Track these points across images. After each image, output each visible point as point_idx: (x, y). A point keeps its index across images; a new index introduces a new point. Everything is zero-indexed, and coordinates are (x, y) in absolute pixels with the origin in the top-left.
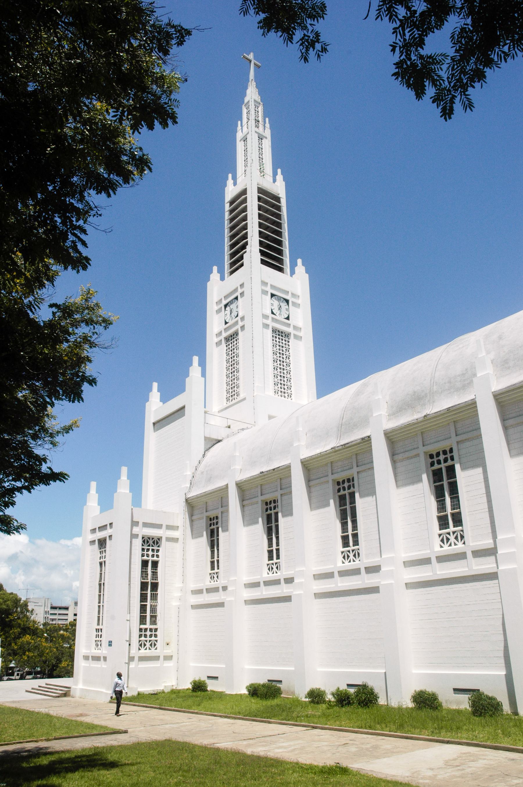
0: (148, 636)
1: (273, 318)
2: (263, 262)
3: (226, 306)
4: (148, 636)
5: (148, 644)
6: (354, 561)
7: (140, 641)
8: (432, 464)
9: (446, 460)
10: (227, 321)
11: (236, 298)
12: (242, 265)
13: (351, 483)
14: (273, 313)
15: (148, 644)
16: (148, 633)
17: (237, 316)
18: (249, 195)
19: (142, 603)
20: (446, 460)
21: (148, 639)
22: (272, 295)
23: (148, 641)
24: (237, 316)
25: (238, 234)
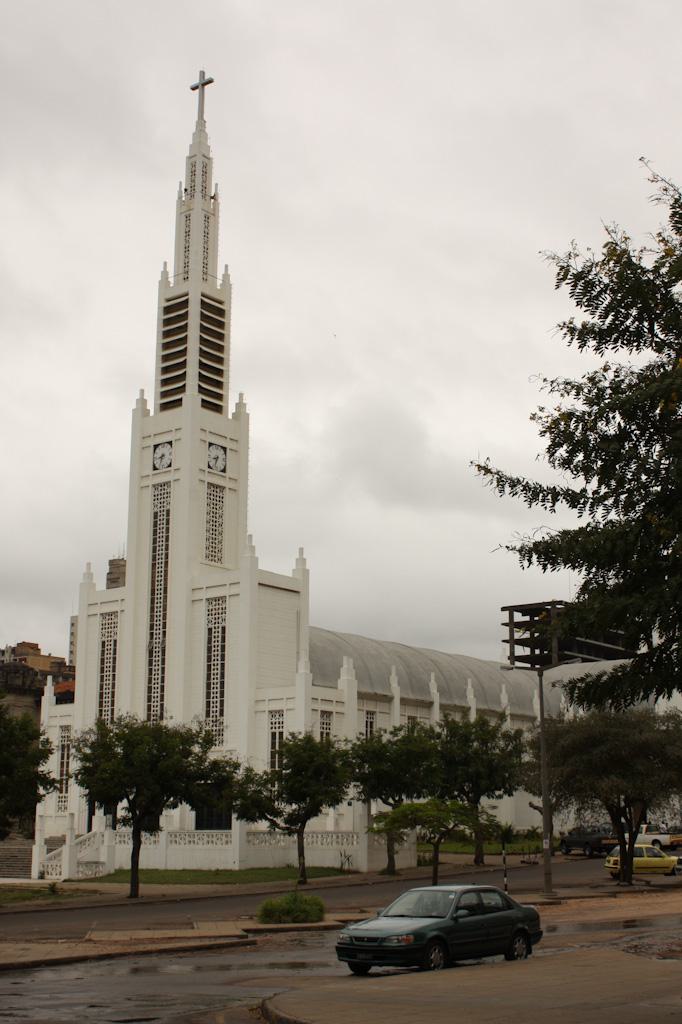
3: (156, 447)
10: (157, 466)
11: (170, 443)
14: (209, 467)
22: (211, 444)
24: (170, 466)
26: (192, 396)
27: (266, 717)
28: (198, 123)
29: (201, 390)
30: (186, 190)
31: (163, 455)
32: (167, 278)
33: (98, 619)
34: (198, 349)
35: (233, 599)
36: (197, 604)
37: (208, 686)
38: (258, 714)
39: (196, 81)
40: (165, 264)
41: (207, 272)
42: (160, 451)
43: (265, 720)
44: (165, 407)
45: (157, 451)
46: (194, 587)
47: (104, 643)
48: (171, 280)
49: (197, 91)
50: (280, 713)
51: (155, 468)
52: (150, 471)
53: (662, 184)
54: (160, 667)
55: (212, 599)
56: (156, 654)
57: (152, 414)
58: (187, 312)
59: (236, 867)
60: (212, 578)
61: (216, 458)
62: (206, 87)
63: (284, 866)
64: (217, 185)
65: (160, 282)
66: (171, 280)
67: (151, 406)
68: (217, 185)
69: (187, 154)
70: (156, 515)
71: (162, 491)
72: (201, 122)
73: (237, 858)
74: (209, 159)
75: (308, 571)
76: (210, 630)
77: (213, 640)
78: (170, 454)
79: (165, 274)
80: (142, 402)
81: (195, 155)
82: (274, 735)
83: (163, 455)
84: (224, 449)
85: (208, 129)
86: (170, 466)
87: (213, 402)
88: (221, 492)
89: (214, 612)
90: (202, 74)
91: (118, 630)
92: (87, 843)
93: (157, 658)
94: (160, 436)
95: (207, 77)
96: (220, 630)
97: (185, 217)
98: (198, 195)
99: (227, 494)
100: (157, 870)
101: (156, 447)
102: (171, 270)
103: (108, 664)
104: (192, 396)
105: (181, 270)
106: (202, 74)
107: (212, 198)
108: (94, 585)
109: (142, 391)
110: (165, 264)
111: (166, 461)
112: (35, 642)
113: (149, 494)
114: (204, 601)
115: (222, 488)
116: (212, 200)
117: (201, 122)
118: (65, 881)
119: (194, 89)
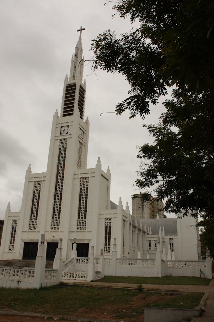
3: (62, 127)
5: (107, 252)
8: (106, 224)
9: (109, 224)
10: (62, 133)
11: (68, 126)
15: (107, 252)
20: (109, 224)
22: (81, 129)
24: (67, 133)
27: (104, 220)
28: (79, 39)
31: (65, 130)
32: (67, 78)
35: (91, 178)
36: (76, 180)
39: (79, 28)
40: (67, 74)
42: (63, 129)
44: (64, 115)
45: (62, 128)
48: (69, 79)
49: (80, 32)
50: (110, 219)
52: (59, 135)
55: (82, 178)
56: (58, 196)
57: (59, 117)
59: (160, 276)
61: (81, 134)
62: (82, 31)
63: (59, 283)
64: (84, 57)
65: (65, 79)
66: (69, 79)
67: (59, 115)
68: (84, 57)
69: (76, 46)
70: (60, 149)
71: (63, 142)
72: (80, 40)
73: (159, 271)
75: (10, 210)
76: (81, 189)
78: (68, 129)
79: (67, 77)
82: (106, 227)
83: (65, 130)
84: (83, 132)
85: (82, 42)
86: (67, 133)
90: (81, 27)
92: (71, 262)
94: (66, 124)
95: (83, 28)
99: (83, 146)
100: (112, 276)
101: (62, 127)
102: (69, 77)
105: (72, 76)
106: (81, 27)
108: (31, 172)
109: (57, 110)
110: (67, 74)
111: (66, 132)
113: (58, 142)
114: (79, 178)
115: (82, 144)
117: (80, 40)
118: (92, 281)
119: (78, 31)
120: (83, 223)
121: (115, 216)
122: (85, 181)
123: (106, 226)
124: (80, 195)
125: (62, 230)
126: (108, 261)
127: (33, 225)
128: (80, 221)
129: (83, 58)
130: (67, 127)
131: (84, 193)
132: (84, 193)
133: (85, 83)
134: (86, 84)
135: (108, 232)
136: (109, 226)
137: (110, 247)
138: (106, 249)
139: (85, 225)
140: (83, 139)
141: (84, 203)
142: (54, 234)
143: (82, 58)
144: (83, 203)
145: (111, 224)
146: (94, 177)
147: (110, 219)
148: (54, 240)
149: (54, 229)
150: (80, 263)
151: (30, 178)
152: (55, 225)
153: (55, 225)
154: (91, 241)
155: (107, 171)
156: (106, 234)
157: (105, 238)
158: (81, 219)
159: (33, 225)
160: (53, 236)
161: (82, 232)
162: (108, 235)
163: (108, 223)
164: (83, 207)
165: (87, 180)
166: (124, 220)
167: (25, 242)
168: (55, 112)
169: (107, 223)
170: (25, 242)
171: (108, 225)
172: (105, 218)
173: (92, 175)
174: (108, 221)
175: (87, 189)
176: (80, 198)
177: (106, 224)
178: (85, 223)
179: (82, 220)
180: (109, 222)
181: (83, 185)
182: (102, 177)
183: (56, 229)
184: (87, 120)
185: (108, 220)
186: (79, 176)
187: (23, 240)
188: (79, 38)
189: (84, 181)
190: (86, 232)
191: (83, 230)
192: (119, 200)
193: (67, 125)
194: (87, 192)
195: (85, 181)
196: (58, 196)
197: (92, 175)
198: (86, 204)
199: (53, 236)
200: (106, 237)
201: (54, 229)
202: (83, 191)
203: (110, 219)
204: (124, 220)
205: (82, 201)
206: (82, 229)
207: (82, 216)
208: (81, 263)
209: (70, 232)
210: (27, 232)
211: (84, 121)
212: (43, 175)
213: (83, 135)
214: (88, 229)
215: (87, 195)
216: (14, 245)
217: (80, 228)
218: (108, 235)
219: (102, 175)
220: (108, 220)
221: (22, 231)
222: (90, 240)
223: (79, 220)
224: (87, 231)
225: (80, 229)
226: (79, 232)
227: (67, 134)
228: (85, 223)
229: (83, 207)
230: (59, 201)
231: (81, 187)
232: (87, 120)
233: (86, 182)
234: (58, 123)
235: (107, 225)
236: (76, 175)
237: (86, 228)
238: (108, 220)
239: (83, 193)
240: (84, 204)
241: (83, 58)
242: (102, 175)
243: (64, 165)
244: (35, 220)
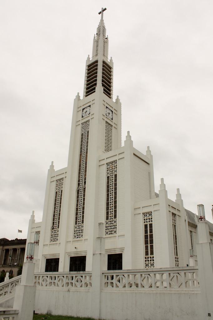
0: (149, 261)
1: (106, 117)
2: (104, 93)
3: (83, 109)
4: (149, 261)
5: (150, 265)
6: (151, 267)
7: (146, 263)
8: (145, 222)
9: (149, 221)
10: (84, 116)
11: (90, 106)
12: (95, 92)
13: (82, 231)
14: (106, 115)
15: (150, 265)
16: (149, 259)
17: (90, 114)
18: (99, 63)
19: (52, 270)
20: (149, 221)
21: (149, 262)
22: (107, 107)
23: (149, 263)
24: (90, 114)
25: (93, 79)
26: (99, 88)
27: (141, 217)
29: (103, 85)
30: (97, 34)
31: (86, 111)
33: (55, 182)
34: (102, 76)
36: (101, 167)
37: (108, 204)
38: (136, 216)
41: (105, 53)
42: (85, 111)
43: (141, 218)
46: (100, 160)
47: (56, 192)
49: (101, 14)
50: (150, 213)
51: (83, 117)
52: (81, 118)
53: (10, 285)
54: (58, 221)
55: (109, 163)
56: (81, 192)
58: (97, 79)
60: (108, 157)
62: (104, 12)
64: (107, 36)
65: (87, 61)
68: (107, 36)
69: (97, 27)
70: (82, 135)
71: (86, 124)
74: (105, 28)
76: (108, 177)
77: (56, 211)
78: (90, 110)
80: (78, 96)
81: (100, 26)
82: (146, 226)
83: (86, 111)
87: (108, 91)
88: (111, 126)
89: (77, 232)
91: (63, 186)
93: (81, 194)
95: (104, 8)
96: (114, 176)
97: (96, 42)
98: (101, 35)
99: (113, 129)
101: (83, 109)
103: (58, 201)
104: (99, 88)
107: (106, 39)
111: (88, 113)
112: (160, 179)
113: (79, 128)
115: (112, 126)
116: (106, 39)
119: (100, 13)
120: (113, 225)
121: (156, 208)
122: (113, 167)
123: (116, 218)
124: (108, 187)
125: (86, 238)
126: (158, 276)
127: (54, 237)
128: (109, 223)
129: (107, 37)
130: (89, 107)
131: (112, 183)
132: (112, 183)
133: (111, 60)
134: (113, 62)
135: (149, 233)
136: (150, 224)
137: (153, 257)
138: (148, 261)
139: (115, 227)
140: (112, 119)
141: (113, 196)
142: (77, 244)
143: (106, 37)
144: (112, 196)
145: (152, 221)
146: (124, 158)
147: (150, 213)
148: (77, 252)
149: (78, 237)
150: (114, 285)
151: (52, 178)
152: (78, 233)
153: (78, 233)
154: (125, 249)
155: (147, 153)
156: (146, 237)
157: (145, 244)
158: (110, 219)
159: (54, 237)
160: (75, 248)
161: (112, 238)
162: (149, 239)
163: (148, 220)
164: (112, 201)
165: (116, 165)
166: (174, 215)
167: (71, 257)
168: (76, 96)
169: (146, 221)
170: (71, 257)
171: (148, 223)
172: (143, 214)
173: (121, 156)
174: (148, 218)
175: (116, 176)
176: (108, 191)
177: (145, 222)
178: (115, 224)
179: (111, 220)
180: (149, 219)
181: (111, 172)
182: (135, 156)
183: (79, 237)
184: (118, 100)
185: (148, 215)
186: (105, 162)
187: (68, 253)
188: (101, 19)
189: (112, 166)
190: (117, 236)
191: (113, 235)
192: (127, 135)
193: (88, 105)
194: (116, 180)
195: (113, 167)
196: (81, 192)
197: (121, 156)
198: (115, 198)
199: (75, 248)
200: (146, 242)
201: (78, 237)
202: (111, 180)
203: (150, 213)
204: (174, 215)
205: (110, 195)
206: (112, 234)
207: (111, 215)
208: (117, 286)
209: (67, 242)
210: (48, 245)
211: (114, 100)
212: (64, 172)
213: (112, 115)
214: (119, 233)
215: (116, 185)
216: (154, 255)
217: (109, 233)
218: (149, 239)
219: (134, 154)
220: (148, 215)
221: (43, 245)
222: (123, 249)
223: (107, 221)
224: (118, 236)
225: (110, 234)
226: (109, 238)
227: (89, 115)
228: (115, 224)
229: (112, 202)
230: (113, 210)
231: (108, 175)
232: (118, 100)
233: (114, 168)
234: (79, 107)
235: (146, 223)
236: (101, 161)
237: (117, 232)
238: (148, 215)
239: (111, 182)
240: (112, 198)
241: (107, 37)
242: (134, 154)
243: (87, 153)
244: (57, 229)
